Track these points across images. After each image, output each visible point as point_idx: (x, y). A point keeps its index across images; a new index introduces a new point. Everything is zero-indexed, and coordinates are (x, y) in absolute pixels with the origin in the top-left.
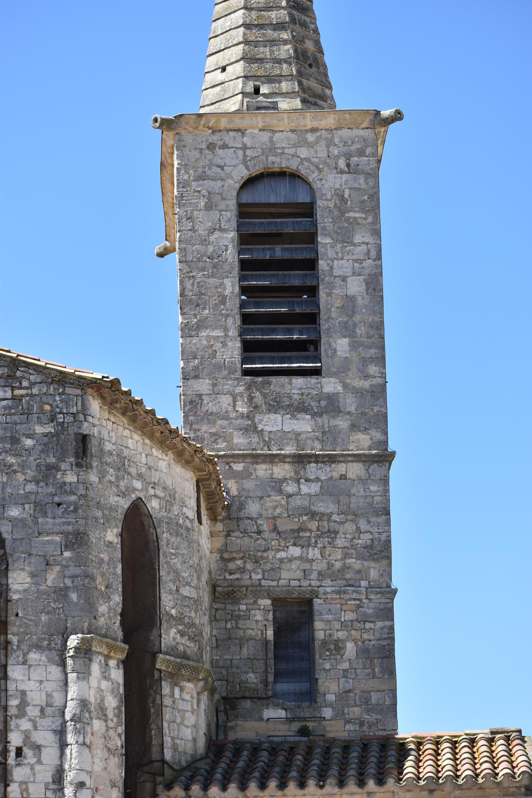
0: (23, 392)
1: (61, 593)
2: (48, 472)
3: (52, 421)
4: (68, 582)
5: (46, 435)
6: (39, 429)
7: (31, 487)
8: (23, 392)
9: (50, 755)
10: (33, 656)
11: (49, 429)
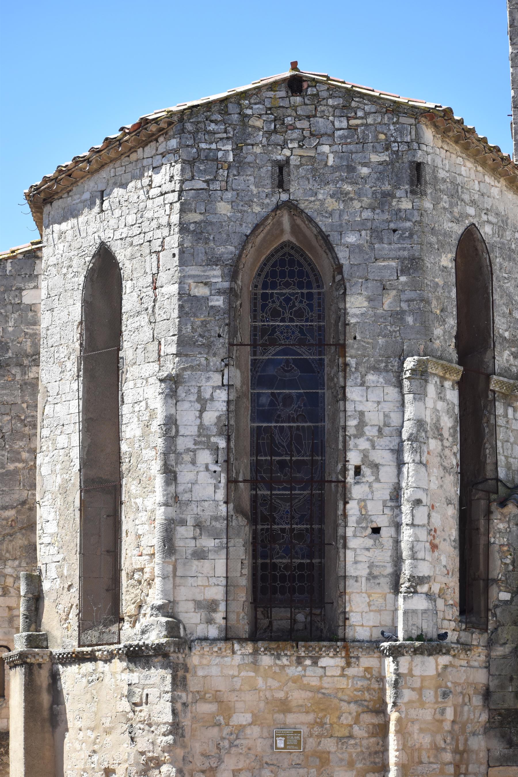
0: (358, 122)
1: (398, 316)
2: (383, 200)
3: (387, 149)
4: (404, 306)
5: (381, 163)
6: (374, 158)
7: (367, 214)
8: (358, 122)
9: (388, 473)
10: (371, 378)
11: (384, 157)
